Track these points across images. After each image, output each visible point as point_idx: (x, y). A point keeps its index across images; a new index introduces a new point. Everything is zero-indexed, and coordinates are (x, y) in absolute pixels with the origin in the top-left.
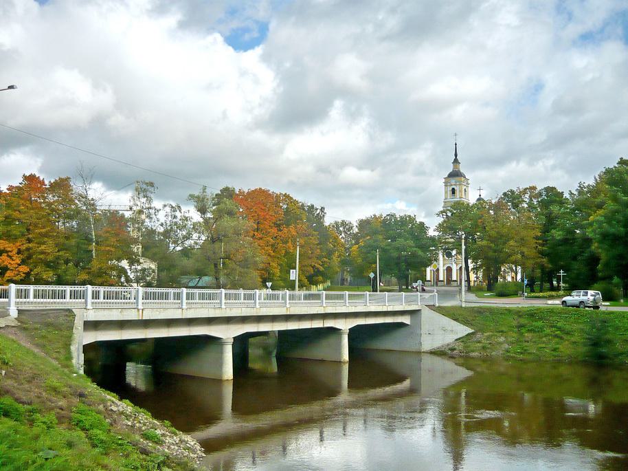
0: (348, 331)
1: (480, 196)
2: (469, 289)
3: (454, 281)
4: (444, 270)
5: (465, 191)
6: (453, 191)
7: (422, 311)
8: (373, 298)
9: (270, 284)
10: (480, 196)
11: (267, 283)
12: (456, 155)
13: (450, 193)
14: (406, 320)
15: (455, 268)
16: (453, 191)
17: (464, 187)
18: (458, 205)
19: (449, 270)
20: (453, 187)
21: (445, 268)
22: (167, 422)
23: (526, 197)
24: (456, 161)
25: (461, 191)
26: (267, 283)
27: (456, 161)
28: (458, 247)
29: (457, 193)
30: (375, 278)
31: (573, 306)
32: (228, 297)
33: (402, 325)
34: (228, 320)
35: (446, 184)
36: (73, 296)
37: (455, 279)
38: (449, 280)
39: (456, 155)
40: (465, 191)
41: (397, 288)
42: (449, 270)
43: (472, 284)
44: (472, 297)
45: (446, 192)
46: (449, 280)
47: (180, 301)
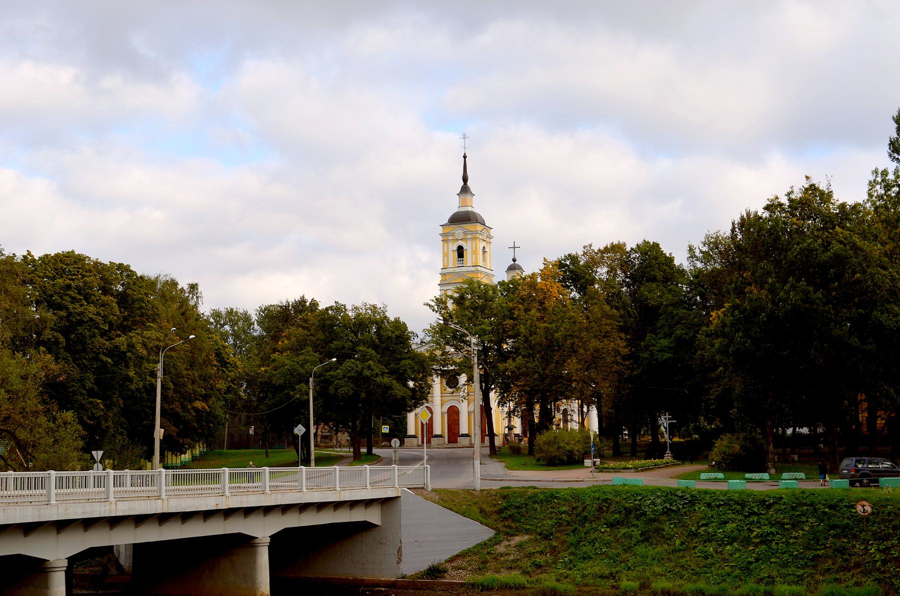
0: (268, 540)
1: (514, 260)
2: (494, 452)
3: (463, 435)
4: (442, 414)
5: (484, 252)
6: (460, 252)
7: (404, 504)
8: (378, 477)
9: (100, 453)
10: (514, 260)
11: (94, 453)
12: (465, 179)
13: (454, 255)
14: (373, 516)
15: (464, 409)
16: (460, 252)
17: (482, 244)
18: (473, 286)
19: (453, 414)
20: (461, 243)
21: (445, 409)
22: (352, 578)
23: (602, 272)
24: (465, 190)
25: (475, 253)
26: (94, 453)
27: (465, 190)
28: (466, 367)
29: (468, 254)
30: (306, 435)
31: (628, 468)
32: (60, 483)
33: (366, 527)
34: (61, 526)
35: (446, 238)
36: (4, 481)
37: (466, 432)
38: (454, 434)
39: (465, 179)
40: (484, 252)
41: (348, 451)
42: (453, 414)
43: (498, 442)
44: (497, 468)
45: (445, 255)
46: (454, 434)
47: (45, 492)
